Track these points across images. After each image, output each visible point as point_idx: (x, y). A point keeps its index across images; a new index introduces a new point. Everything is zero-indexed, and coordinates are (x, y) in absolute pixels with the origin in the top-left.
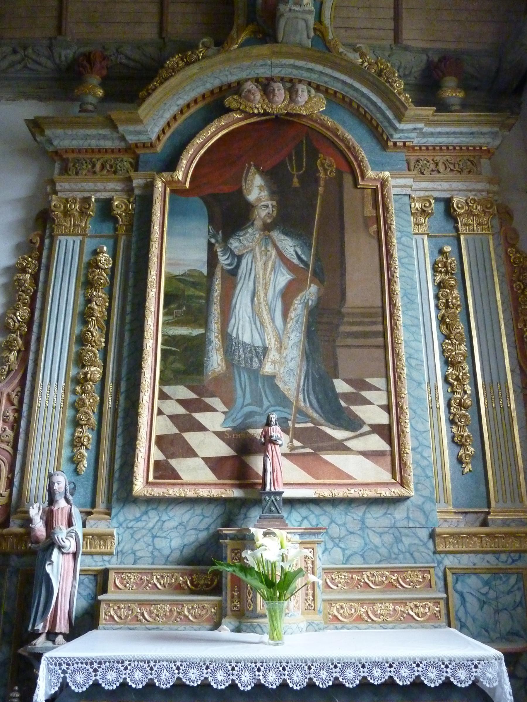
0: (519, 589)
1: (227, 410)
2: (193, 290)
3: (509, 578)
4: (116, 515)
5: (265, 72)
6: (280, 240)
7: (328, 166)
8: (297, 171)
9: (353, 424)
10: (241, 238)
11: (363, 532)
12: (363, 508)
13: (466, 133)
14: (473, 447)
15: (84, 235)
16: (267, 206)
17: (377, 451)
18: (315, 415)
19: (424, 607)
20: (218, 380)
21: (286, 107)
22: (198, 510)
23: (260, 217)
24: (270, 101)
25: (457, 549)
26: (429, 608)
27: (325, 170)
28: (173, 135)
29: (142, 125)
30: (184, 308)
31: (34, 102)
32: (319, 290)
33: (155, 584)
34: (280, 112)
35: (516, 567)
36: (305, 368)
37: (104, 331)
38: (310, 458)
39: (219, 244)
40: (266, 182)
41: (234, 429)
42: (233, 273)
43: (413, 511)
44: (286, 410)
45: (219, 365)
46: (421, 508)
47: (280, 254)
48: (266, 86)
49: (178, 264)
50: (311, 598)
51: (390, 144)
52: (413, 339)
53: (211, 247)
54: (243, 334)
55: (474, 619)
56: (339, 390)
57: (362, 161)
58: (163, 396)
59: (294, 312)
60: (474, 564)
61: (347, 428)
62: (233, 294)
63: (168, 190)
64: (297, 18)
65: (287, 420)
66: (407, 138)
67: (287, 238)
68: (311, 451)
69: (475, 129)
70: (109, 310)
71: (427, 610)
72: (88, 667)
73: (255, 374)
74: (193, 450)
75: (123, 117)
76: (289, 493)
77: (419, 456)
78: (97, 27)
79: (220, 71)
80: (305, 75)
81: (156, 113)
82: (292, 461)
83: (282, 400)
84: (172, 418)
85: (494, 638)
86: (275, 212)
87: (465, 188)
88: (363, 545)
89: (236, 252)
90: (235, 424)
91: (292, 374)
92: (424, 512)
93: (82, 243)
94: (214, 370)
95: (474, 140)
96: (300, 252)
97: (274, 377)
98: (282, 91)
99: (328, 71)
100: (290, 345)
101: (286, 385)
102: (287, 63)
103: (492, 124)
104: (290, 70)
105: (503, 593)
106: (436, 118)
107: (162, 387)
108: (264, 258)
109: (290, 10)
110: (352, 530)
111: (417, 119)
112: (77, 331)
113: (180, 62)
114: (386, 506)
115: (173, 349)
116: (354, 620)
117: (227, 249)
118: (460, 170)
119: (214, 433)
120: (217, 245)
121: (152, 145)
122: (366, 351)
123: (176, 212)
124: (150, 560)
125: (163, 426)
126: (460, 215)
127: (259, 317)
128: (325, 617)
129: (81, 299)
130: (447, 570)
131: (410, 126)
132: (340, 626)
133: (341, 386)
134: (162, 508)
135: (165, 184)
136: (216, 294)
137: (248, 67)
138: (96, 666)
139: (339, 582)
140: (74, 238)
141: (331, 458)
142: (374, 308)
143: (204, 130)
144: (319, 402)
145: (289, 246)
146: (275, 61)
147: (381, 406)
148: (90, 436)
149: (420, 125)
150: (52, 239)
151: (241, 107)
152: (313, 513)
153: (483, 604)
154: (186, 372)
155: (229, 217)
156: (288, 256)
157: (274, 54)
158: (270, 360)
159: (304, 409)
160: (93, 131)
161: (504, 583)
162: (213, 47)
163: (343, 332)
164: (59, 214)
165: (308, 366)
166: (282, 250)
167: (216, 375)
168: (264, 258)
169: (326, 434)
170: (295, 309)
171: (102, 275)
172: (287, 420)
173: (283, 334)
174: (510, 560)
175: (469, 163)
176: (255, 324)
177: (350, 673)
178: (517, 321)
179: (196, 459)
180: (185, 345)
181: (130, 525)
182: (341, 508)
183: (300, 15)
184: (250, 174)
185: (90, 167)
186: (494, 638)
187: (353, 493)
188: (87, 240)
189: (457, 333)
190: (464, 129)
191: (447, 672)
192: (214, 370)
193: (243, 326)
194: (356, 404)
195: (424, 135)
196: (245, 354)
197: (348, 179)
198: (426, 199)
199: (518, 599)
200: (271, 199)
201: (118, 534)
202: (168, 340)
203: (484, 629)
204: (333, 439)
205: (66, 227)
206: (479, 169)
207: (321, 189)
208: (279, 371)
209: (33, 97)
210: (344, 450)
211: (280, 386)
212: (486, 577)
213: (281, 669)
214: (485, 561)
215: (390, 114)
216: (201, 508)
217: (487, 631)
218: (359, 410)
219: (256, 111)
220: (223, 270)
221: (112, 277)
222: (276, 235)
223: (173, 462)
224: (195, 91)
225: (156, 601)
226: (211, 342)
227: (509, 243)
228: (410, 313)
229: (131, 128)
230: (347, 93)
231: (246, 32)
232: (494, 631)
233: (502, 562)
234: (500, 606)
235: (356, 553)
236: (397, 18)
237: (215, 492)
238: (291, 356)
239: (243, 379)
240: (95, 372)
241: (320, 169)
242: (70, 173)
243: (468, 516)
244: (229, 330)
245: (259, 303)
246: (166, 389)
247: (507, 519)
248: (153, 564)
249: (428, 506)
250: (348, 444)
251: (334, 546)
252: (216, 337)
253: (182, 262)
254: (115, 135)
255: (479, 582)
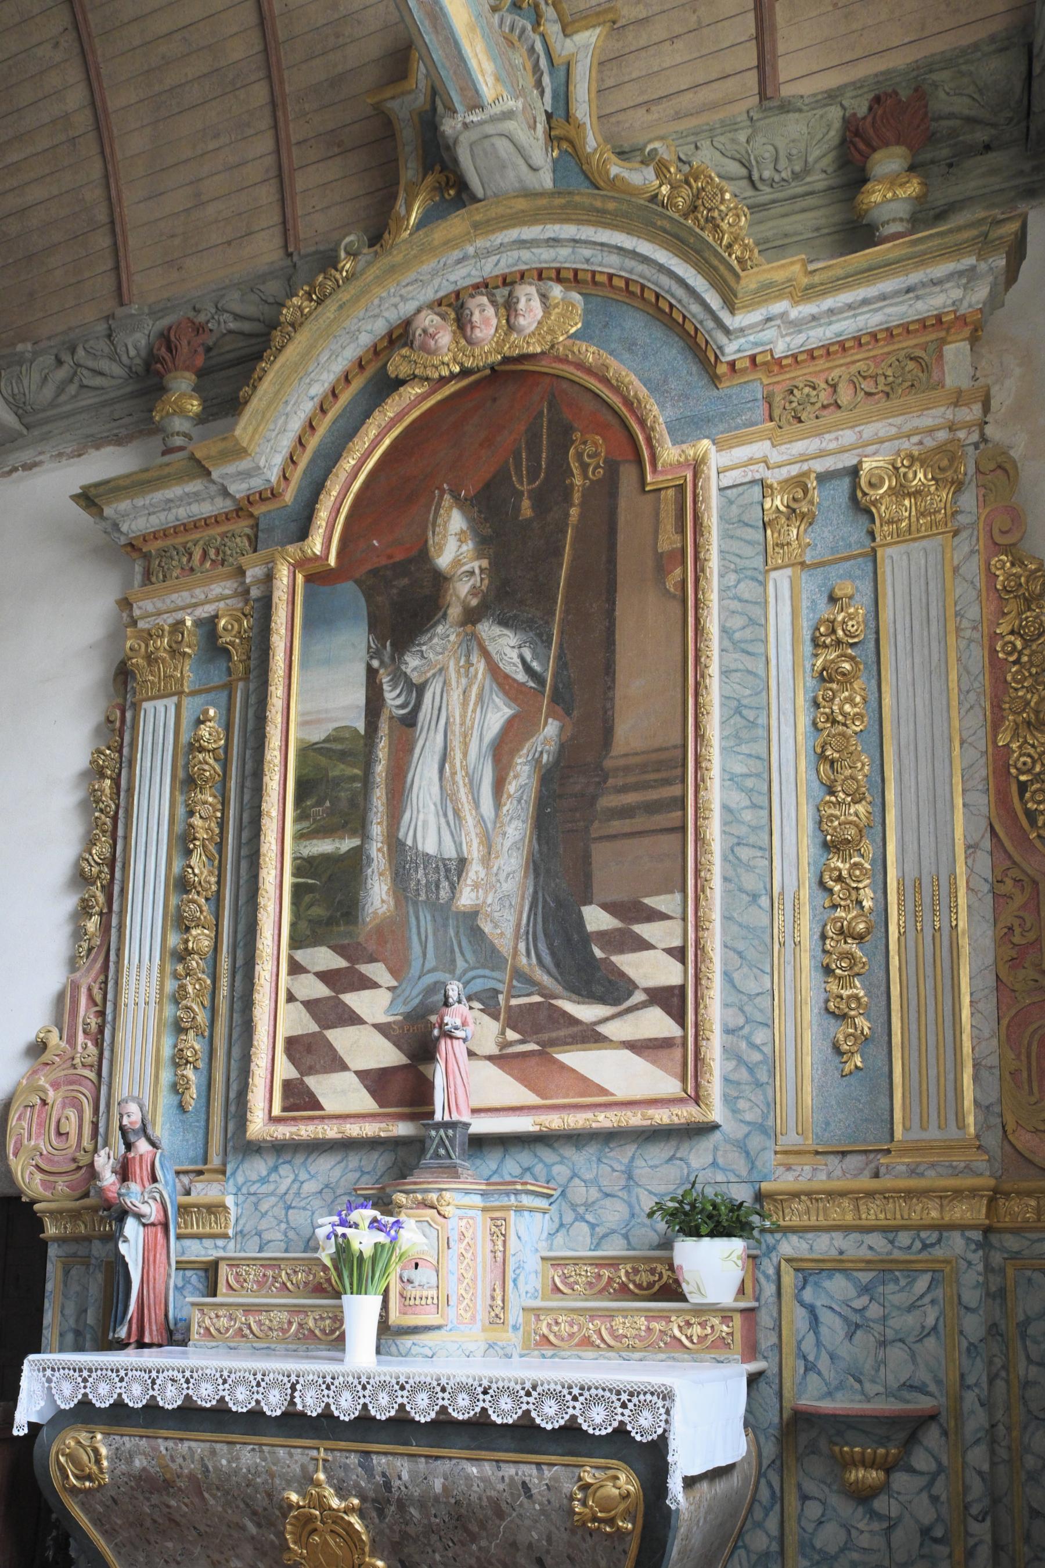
0: (933, 1302)
1: (395, 983)
2: (342, 766)
3: (914, 1280)
4: (233, 1174)
5: (469, 275)
6: (494, 639)
7: (589, 456)
8: (530, 483)
9: (613, 989)
10: (424, 648)
11: (629, 1192)
12: (630, 1149)
13: (896, 293)
14: (868, 1019)
15: (180, 693)
16: (472, 573)
17: (656, 1039)
18: (546, 980)
19: (703, 1325)
20: (381, 932)
21: (501, 344)
22: (354, 1160)
23: (458, 597)
24: (470, 342)
25: (807, 1223)
26: (712, 1327)
27: (584, 467)
28: (312, 461)
29: (249, 458)
30: (328, 804)
31: (110, 449)
32: (562, 729)
33: (284, 1284)
34: (490, 360)
35: (930, 1257)
36: (531, 890)
37: (216, 862)
38: (533, 1061)
39: (386, 668)
40: (470, 520)
41: (408, 1017)
42: (410, 721)
43: (725, 1151)
44: (494, 974)
45: (383, 901)
46: (741, 1146)
47: (494, 670)
48: (455, 307)
49: (319, 721)
50: (500, 1303)
51: (722, 369)
52: (748, 803)
53: (372, 674)
54: (424, 838)
55: (832, 1357)
56: (591, 927)
57: (653, 429)
58: (296, 968)
59: (514, 783)
60: (841, 1253)
61: (602, 1000)
62: (409, 763)
63: (300, 578)
64: (487, 137)
65: (496, 992)
66: (756, 344)
67: (506, 632)
68: (536, 1047)
69: (915, 277)
70: (222, 824)
71: (709, 1330)
72: (77, 1374)
73: (442, 911)
74: (341, 1060)
75: (214, 451)
76: (481, 1126)
77: (744, 1045)
78: (180, 269)
79: (381, 299)
80: (528, 259)
81: (272, 427)
82: (501, 1068)
83: (489, 956)
84: (311, 1006)
85: (872, 1394)
86: (486, 582)
87: (894, 431)
88: (627, 1216)
89: (416, 678)
90: (408, 1009)
91: (507, 904)
92: (747, 1153)
93: (178, 707)
94: (375, 913)
95: (920, 305)
96: (528, 657)
97: (476, 913)
98: (490, 311)
99: (588, 232)
100: (505, 849)
101: (496, 926)
102: (506, 240)
103: (955, 251)
104: (515, 254)
105: (899, 1308)
106: (817, 279)
107: (293, 952)
108: (464, 681)
109: (466, 125)
110: (608, 1190)
111: (767, 292)
112: (176, 869)
113: (306, 303)
114: (673, 1143)
115: (310, 881)
116: (577, 1345)
117: (399, 676)
118: (887, 389)
119: (376, 1026)
120: (382, 671)
121: (274, 494)
122: (646, 841)
123: (317, 619)
124: (283, 1245)
125: (294, 1021)
126: (874, 503)
127: (451, 801)
128: (527, 1335)
129: (181, 810)
130: (783, 1263)
131: (755, 316)
132: (549, 1353)
133: (597, 918)
134: (299, 1159)
135: (297, 566)
136: (380, 769)
137: (434, 274)
138: (85, 1374)
139: (577, 1283)
140: (165, 701)
141: (573, 1058)
142: (667, 749)
143: (356, 440)
144: (553, 954)
145: (507, 646)
146: (481, 243)
147: (669, 951)
148: (197, 1047)
149: (779, 307)
150: (136, 707)
151: (417, 372)
152: (541, 1160)
153: (853, 1329)
154: (330, 922)
155: (401, 607)
156: (508, 669)
157: (482, 227)
158: (469, 882)
159: (527, 970)
160: (176, 491)
161: (902, 1290)
162: (365, 250)
163: (605, 808)
164: (140, 661)
165: (536, 886)
166: (496, 657)
167: (377, 921)
168: (464, 681)
169: (565, 1013)
170: (515, 777)
171: (207, 763)
172: (496, 992)
173: (494, 828)
174: (918, 1245)
175: (911, 365)
176: (445, 815)
177: (422, 1399)
178: (996, 727)
179: (346, 1074)
180: (329, 872)
181: (252, 1190)
182: (591, 1150)
183: (490, 129)
184: (442, 511)
185: (185, 560)
186: (872, 1394)
187: (604, 1120)
188: (186, 701)
189: (846, 779)
190: (887, 286)
191: (574, 1408)
192: (375, 913)
193: (425, 822)
194: (622, 952)
195: (797, 326)
196: (426, 875)
197: (627, 475)
198: (799, 483)
199: (930, 1321)
200: (479, 556)
201: (237, 1205)
202: (305, 866)
203: (853, 1376)
204: (573, 1021)
205: (152, 683)
206: (935, 376)
207: (574, 512)
208: (484, 902)
209: (109, 443)
210: (596, 1041)
211: (486, 930)
212: (865, 1277)
213: (324, 1387)
214: (865, 1246)
215: (714, 300)
216: (357, 1158)
217: (860, 1382)
218: (629, 963)
219: (445, 372)
220: (391, 718)
221: (225, 765)
222: (487, 630)
223: (311, 1081)
224: (340, 359)
225: (267, 1305)
226: (370, 861)
227: (996, 544)
228: (744, 749)
229: (231, 469)
230: (631, 272)
231: (420, 198)
232: (873, 1381)
233: (900, 1248)
234: (890, 1334)
235: (614, 1232)
236: (763, 35)
237: (369, 1129)
238: (508, 869)
239: (422, 923)
240: (201, 938)
241: (574, 466)
242: (154, 579)
243: (849, 1158)
244: (401, 835)
245: (454, 774)
246: (300, 955)
247: (918, 1164)
248: (286, 1251)
249: (756, 1142)
250: (604, 1029)
251: (576, 1219)
252: (379, 850)
253: (323, 716)
254: (213, 489)
255: (850, 1285)
